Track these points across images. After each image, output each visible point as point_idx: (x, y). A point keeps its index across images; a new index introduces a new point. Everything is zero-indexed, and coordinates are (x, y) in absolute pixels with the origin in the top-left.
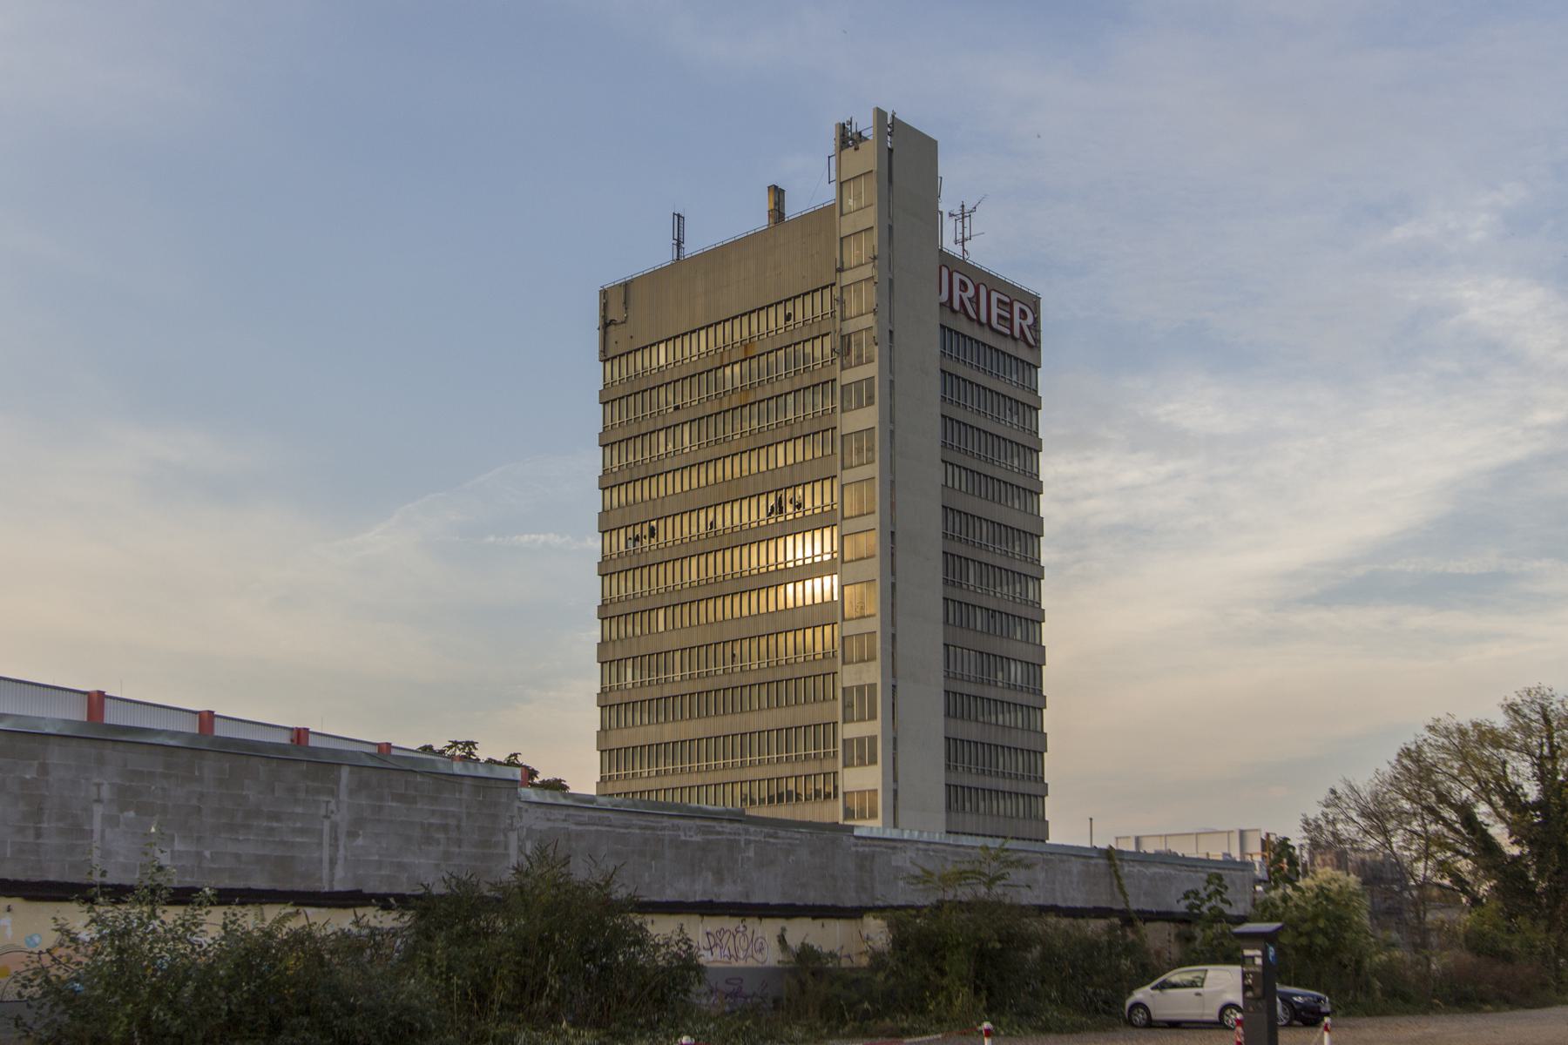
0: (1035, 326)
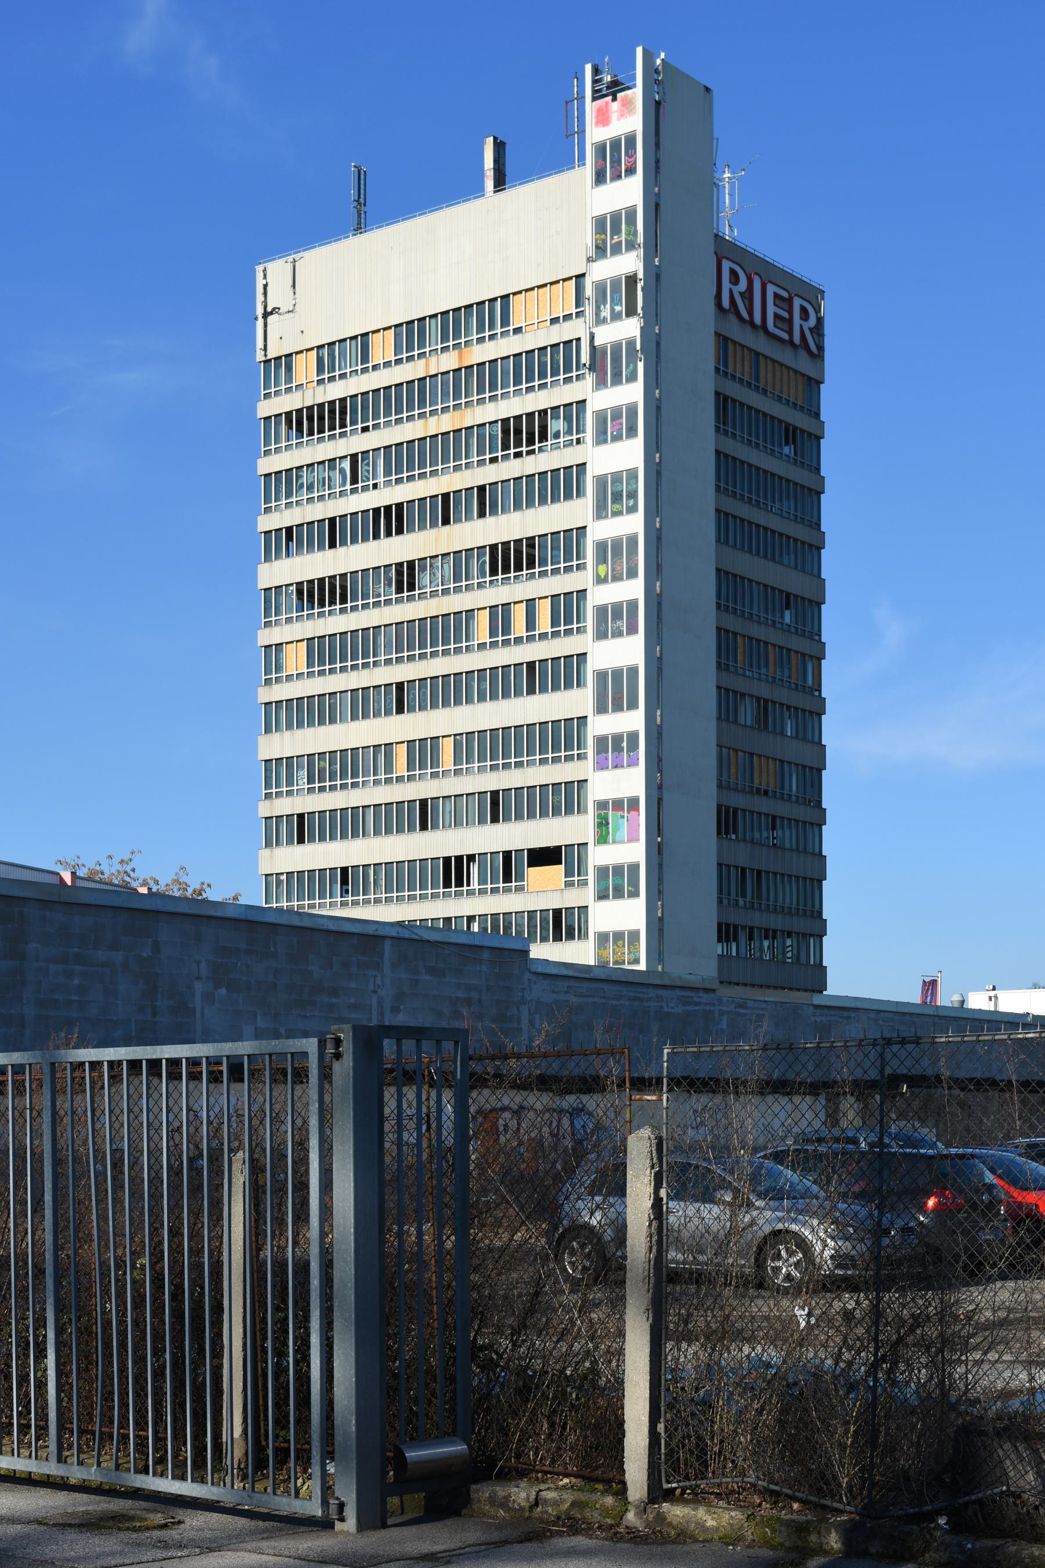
0: (818, 330)
